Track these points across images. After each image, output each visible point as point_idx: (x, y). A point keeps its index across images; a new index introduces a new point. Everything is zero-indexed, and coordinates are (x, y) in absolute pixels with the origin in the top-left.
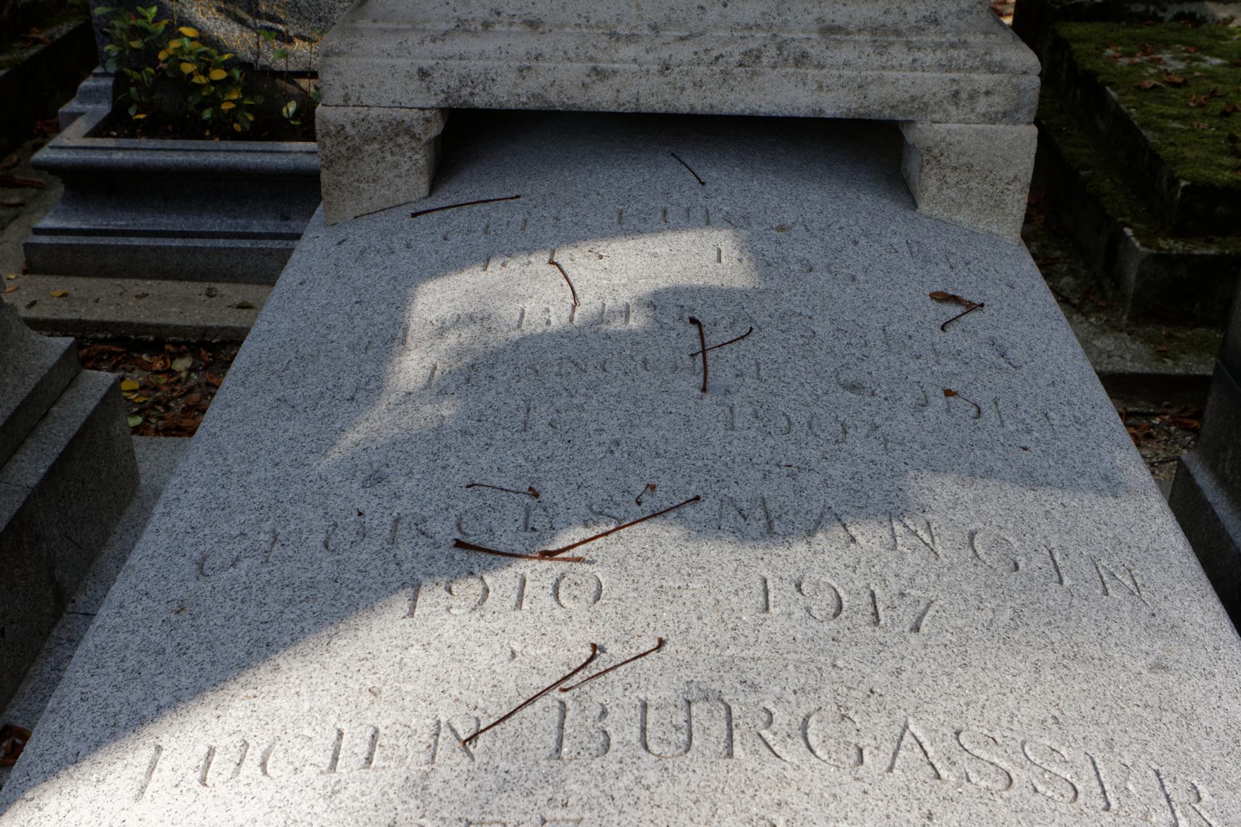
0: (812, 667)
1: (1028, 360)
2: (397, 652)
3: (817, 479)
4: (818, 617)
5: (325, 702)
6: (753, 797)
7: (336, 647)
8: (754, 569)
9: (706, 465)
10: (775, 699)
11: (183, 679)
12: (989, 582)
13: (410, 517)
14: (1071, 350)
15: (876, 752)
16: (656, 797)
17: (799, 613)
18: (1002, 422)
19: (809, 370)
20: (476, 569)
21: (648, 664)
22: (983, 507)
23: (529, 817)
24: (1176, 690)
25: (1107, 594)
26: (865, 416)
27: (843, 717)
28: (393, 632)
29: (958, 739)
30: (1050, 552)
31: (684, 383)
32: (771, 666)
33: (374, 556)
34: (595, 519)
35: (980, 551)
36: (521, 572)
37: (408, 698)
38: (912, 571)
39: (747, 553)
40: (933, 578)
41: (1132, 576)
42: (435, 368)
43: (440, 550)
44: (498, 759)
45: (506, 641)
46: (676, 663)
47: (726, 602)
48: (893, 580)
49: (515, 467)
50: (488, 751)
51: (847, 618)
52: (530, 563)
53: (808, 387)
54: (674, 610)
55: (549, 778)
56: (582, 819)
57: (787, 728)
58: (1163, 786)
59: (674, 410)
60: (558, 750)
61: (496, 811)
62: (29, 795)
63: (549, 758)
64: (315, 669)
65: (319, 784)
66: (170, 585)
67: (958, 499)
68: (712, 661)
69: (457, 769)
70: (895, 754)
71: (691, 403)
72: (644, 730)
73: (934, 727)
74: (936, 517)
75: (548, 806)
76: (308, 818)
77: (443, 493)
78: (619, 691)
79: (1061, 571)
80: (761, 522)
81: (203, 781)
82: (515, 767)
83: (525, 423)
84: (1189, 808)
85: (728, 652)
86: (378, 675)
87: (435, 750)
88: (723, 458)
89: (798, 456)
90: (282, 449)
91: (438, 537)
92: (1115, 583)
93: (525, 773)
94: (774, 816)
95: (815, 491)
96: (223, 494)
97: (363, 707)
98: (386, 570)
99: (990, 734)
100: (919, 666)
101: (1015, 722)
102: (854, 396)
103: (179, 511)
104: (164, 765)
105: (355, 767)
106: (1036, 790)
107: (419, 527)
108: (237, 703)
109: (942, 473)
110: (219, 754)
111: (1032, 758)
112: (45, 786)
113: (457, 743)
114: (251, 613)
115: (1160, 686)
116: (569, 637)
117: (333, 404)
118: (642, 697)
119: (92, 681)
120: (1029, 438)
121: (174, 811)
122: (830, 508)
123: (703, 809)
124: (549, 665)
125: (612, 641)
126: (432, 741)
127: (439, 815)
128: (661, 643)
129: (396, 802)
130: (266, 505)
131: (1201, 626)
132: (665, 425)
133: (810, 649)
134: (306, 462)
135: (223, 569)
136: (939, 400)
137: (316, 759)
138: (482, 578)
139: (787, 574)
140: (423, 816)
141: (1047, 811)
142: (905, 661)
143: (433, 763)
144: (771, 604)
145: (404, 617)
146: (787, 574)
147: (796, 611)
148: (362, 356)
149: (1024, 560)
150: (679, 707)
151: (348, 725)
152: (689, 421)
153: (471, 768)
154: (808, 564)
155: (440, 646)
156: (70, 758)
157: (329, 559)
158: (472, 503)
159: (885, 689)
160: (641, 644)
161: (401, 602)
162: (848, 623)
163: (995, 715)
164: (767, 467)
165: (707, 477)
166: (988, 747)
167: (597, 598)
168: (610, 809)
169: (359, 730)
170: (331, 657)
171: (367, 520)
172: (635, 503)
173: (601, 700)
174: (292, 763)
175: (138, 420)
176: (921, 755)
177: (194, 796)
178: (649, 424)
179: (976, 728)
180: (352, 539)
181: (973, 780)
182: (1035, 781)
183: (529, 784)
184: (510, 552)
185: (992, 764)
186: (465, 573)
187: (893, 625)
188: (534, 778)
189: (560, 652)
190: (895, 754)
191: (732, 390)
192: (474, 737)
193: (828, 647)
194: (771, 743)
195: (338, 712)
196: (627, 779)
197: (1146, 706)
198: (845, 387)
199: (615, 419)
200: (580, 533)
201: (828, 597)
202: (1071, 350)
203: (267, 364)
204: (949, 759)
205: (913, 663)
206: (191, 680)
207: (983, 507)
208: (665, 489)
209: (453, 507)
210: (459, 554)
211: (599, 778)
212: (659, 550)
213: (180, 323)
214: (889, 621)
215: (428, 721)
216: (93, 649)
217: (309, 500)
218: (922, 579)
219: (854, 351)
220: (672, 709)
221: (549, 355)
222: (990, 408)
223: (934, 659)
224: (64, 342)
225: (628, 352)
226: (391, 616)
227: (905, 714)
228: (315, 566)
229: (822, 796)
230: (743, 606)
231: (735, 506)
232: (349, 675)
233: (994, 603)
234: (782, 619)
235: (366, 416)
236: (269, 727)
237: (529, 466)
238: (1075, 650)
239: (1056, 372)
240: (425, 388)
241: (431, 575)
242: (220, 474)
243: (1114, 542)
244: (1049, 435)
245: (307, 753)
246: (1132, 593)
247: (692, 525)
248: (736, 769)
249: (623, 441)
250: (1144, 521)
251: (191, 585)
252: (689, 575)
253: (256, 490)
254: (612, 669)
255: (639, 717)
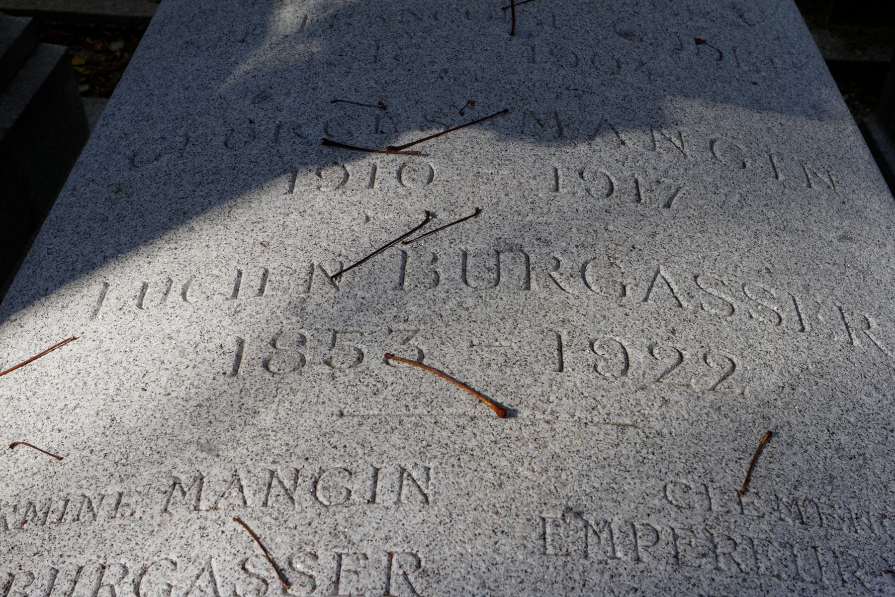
0: (590, 230)
1: (760, 20)
2: (281, 217)
3: (597, 99)
4: (596, 196)
5: (227, 252)
6: (545, 316)
7: (235, 214)
8: (548, 161)
9: (513, 88)
10: (562, 251)
11: (122, 238)
12: (724, 175)
13: (288, 124)
14: (792, 15)
15: (635, 288)
16: (473, 315)
17: (581, 193)
18: (738, 64)
19: (593, 21)
20: (339, 160)
21: (468, 226)
22: (721, 123)
23: (379, 328)
24: (857, 254)
25: (811, 187)
26: (635, 55)
27: (612, 264)
28: (277, 204)
29: (696, 281)
30: (770, 157)
31: (497, 29)
32: (560, 228)
33: (262, 151)
34: (429, 125)
35: (718, 154)
36: (372, 162)
37: (290, 248)
38: (667, 166)
39: (543, 151)
40: (682, 171)
41: (829, 175)
42: (306, 18)
43: (312, 147)
44: (357, 289)
45: (362, 210)
46: (488, 225)
47: (527, 184)
48: (651, 171)
49: (369, 88)
50: (349, 284)
51: (616, 197)
52: (379, 156)
53: (591, 33)
54: (488, 189)
55: (395, 302)
56: (419, 330)
57: (570, 271)
58: (843, 318)
59: (489, 48)
60: (401, 283)
61: (356, 324)
62: (13, 317)
63: (394, 289)
64: (220, 230)
65: (225, 307)
66: (110, 174)
67: (703, 117)
68: (516, 224)
69: (326, 296)
70: (649, 290)
71: (502, 43)
72: (464, 271)
73: (678, 272)
74: (686, 129)
75: (394, 321)
76: (218, 329)
77: (314, 107)
78: (446, 244)
79: (777, 170)
80: (555, 129)
81: (140, 306)
82: (369, 295)
83: (375, 57)
84: (862, 332)
85: (528, 219)
86: (267, 233)
87: (310, 284)
88: (526, 83)
89: (583, 83)
90: (190, 77)
91: (310, 138)
92: (817, 180)
93: (376, 299)
94: (560, 329)
95: (595, 107)
96: (147, 110)
97: (257, 254)
98: (271, 161)
99: (719, 279)
100: (669, 231)
101: (739, 271)
102: (627, 41)
103: (115, 123)
104: (111, 295)
105: (251, 295)
106: (751, 317)
107: (296, 131)
108: (163, 253)
109: (691, 98)
110: (151, 287)
111: (750, 295)
112: (25, 311)
113: (326, 278)
114: (171, 192)
115: (845, 251)
116: (409, 207)
117: (229, 44)
118: (463, 248)
119: (55, 241)
120: (758, 76)
121: (119, 325)
122: (606, 120)
123: (507, 324)
124: (394, 226)
125: (441, 210)
126: (307, 278)
127: (314, 327)
128: (478, 211)
129: (282, 318)
130: (179, 117)
131: (878, 212)
132: (482, 58)
133: (588, 218)
134: (209, 86)
135: (149, 162)
136: (691, 46)
137: (222, 290)
138: (343, 167)
139: (573, 165)
140: (302, 327)
141: (759, 331)
142: (659, 228)
143: (309, 292)
144: (560, 186)
145: (285, 194)
146: (573, 165)
147: (579, 191)
148: (250, 9)
149: (750, 161)
150: (491, 255)
151: (246, 267)
152: (501, 56)
153: (336, 295)
154: (589, 159)
155: (312, 213)
156: (42, 292)
157: (229, 154)
158: (336, 114)
159: (643, 246)
160: (463, 212)
161: (283, 184)
162: (617, 200)
163: (724, 266)
164: (559, 90)
165: (514, 96)
166: (717, 287)
167: (430, 180)
168: (440, 323)
169: (254, 270)
170: (231, 221)
171: (256, 126)
172: (459, 114)
173: (433, 250)
174: (205, 293)
175: (85, 88)
176: (669, 291)
177: (133, 315)
178: (470, 58)
179: (709, 274)
180: (245, 140)
181: (706, 309)
182: (751, 311)
183: (380, 307)
184: (365, 148)
185: (720, 298)
186: (331, 163)
187: (651, 203)
188: (383, 303)
189: (402, 218)
190: (649, 290)
191: (534, 34)
192: (339, 275)
193: (602, 216)
194: (559, 281)
195: (237, 258)
196: (452, 304)
197: (835, 264)
198: (620, 34)
199: (444, 54)
200: (417, 135)
201: (603, 182)
202: (792, 15)
203: (177, 18)
204: (689, 294)
205: (665, 229)
206: (128, 238)
207: (721, 123)
208: (482, 105)
209: (321, 117)
210: (326, 150)
211: (431, 303)
212: (477, 147)
213: (113, 13)
214: (648, 200)
215: (305, 264)
216: (55, 219)
217: (212, 113)
218: (674, 172)
219: (627, 9)
220: (485, 256)
221: (394, 8)
222: (730, 53)
223: (681, 227)
224: (25, 21)
225: (455, 6)
226: (276, 192)
227: (657, 263)
228: (218, 159)
229: (595, 317)
230: (539, 187)
231: (534, 117)
232: (246, 233)
233: (727, 190)
234: (568, 197)
235: (254, 53)
236: (187, 269)
237: (378, 87)
238: (785, 224)
239: (781, 30)
240: (299, 32)
241: (305, 164)
242: (144, 96)
243: (817, 152)
244: (773, 75)
245: (216, 286)
246: (829, 187)
247: (502, 130)
248: (532, 298)
249: (450, 70)
250: (840, 138)
251: (126, 174)
252: (499, 165)
253: (172, 106)
254: (441, 229)
255: (461, 261)
